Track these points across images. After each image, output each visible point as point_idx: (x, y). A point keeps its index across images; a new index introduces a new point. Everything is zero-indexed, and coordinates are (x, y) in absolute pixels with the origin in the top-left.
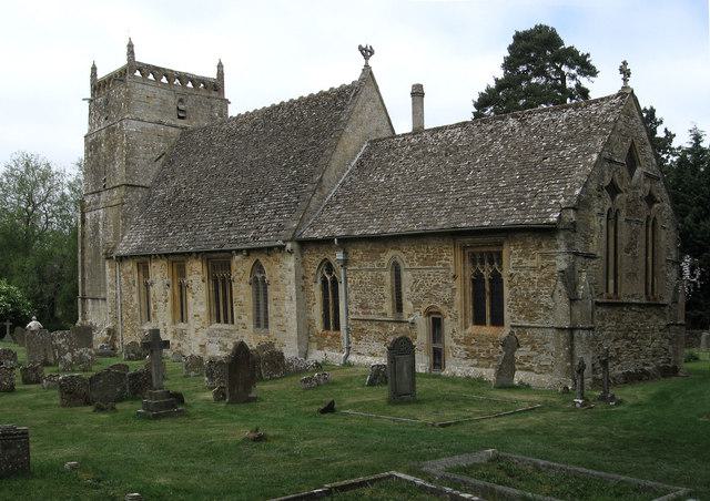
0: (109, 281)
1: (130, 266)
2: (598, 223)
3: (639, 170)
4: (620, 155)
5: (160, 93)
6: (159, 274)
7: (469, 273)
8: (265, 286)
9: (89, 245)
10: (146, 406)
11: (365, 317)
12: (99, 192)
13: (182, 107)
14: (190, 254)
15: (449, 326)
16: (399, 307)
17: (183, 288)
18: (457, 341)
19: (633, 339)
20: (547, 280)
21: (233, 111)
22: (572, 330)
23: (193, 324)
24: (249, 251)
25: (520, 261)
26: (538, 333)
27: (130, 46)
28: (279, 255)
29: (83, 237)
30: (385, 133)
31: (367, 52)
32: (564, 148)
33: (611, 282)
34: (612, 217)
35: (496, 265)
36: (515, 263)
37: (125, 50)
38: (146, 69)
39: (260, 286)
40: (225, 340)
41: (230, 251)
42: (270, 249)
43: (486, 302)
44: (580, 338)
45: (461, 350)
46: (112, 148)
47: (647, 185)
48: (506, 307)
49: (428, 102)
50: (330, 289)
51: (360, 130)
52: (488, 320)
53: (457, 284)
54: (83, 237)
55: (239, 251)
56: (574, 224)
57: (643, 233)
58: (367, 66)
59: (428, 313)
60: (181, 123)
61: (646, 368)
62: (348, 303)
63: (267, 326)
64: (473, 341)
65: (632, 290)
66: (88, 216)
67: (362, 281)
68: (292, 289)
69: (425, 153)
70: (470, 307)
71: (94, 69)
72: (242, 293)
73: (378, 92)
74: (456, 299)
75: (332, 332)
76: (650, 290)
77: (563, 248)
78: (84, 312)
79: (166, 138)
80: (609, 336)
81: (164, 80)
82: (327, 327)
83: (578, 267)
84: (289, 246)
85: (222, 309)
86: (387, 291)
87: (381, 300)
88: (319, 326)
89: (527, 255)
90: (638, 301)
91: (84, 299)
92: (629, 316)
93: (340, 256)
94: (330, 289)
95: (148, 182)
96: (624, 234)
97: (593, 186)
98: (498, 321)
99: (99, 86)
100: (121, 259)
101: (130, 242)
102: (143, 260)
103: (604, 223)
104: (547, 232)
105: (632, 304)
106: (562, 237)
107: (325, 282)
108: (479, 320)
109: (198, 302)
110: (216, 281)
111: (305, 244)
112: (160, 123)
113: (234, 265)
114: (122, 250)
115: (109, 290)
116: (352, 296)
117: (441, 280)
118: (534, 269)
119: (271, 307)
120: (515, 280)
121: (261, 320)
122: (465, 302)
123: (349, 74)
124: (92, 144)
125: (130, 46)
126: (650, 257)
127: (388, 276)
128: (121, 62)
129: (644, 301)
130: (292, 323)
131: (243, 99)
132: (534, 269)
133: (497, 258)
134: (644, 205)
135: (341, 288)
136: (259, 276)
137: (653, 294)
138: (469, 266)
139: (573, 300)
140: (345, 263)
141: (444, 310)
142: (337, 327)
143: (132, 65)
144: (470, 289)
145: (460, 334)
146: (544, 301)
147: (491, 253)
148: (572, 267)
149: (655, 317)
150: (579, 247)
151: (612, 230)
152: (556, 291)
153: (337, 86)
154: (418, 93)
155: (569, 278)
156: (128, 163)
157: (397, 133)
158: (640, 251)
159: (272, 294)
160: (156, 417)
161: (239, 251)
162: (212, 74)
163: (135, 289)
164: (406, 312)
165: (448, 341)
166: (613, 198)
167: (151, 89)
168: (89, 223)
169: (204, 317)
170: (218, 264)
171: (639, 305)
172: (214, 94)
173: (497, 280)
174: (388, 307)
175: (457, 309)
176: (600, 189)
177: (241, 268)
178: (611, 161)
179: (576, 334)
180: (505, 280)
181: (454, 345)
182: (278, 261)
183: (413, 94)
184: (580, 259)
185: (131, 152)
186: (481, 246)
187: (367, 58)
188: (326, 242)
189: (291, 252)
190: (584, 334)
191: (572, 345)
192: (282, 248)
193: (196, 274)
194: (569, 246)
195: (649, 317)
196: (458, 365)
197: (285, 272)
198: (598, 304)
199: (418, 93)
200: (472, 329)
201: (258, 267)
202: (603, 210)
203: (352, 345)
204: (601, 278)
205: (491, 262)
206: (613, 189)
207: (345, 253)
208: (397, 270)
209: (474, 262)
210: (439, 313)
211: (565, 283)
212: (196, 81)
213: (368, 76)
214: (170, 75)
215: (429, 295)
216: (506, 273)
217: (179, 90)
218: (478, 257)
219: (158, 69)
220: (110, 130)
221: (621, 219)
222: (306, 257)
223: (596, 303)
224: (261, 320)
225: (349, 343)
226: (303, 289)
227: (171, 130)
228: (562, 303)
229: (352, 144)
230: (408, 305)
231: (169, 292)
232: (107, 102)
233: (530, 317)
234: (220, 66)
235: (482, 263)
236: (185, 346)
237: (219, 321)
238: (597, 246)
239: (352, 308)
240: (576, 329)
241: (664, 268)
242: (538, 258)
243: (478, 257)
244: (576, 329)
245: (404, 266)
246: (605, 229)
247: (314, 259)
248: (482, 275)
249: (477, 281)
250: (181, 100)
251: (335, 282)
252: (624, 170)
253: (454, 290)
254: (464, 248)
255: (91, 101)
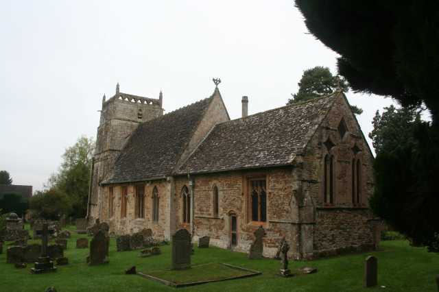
0: (99, 196)
1: (106, 189)
2: (318, 163)
3: (347, 133)
4: (334, 124)
5: (131, 107)
6: (117, 192)
7: (251, 191)
8: (158, 198)
9: (94, 179)
10: (36, 266)
11: (201, 216)
12: (100, 154)
13: (140, 113)
14: (129, 183)
15: (240, 221)
16: (216, 211)
17: (126, 199)
18: (243, 230)
19: (343, 229)
20: (287, 195)
21: (164, 113)
22: (300, 225)
23: (129, 218)
24: (153, 182)
25: (274, 186)
26: (283, 226)
27: (118, 86)
28: (164, 184)
29: (92, 175)
30: (225, 120)
31: (217, 82)
32: (303, 123)
33: (328, 196)
34: (328, 160)
35: (263, 188)
36: (275, 187)
37: (159, 95)
38: (124, 96)
39: (156, 199)
40: (140, 226)
41: (144, 181)
42: (161, 180)
43: (258, 209)
44: (305, 229)
45: (244, 235)
46: (106, 132)
47: (353, 142)
48: (267, 212)
49: (250, 104)
50: (187, 200)
51: (212, 120)
52: (259, 218)
53: (244, 198)
54: (92, 175)
55: (148, 182)
56: (302, 164)
57: (350, 167)
58: (217, 88)
59: (230, 214)
60: (140, 120)
61: (354, 246)
62: (194, 208)
63: (158, 220)
64: (251, 230)
65: (343, 200)
66: (95, 165)
67: (201, 194)
68: (168, 201)
69: (239, 129)
70: (250, 210)
71: (104, 97)
72: (149, 203)
73: (222, 101)
74: (242, 205)
75: (187, 224)
76: (356, 200)
77: (296, 177)
78: (90, 211)
79: (132, 127)
80: (327, 228)
81: (133, 101)
82: (184, 221)
83: (305, 188)
84: (168, 179)
85: (140, 212)
86: (211, 202)
87: (208, 207)
88: (181, 220)
89: (278, 182)
90: (347, 207)
91: (90, 204)
92: (341, 216)
93: (191, 183)
94: (187, 200)
95: (121, 148)
96: (337, 169)
97: (315, 142)
98: (264, 219)
99: (106, 105)
100: (104, 185)
101: (110, 177)
102: (111, 186)
103: (323, 163)
104: (288, 168)
105: (344, 209)
106: (295, 171)
107: (185, 197)
108: (255, 218)
109: (131, 208)
110: (139, 196)
111: (177, 178)
112: (129, 120)
113: (146, 188)
114: (105, 181)
115: (99, 201)
116: (196, 204)
117: (234, 195)
118: (281, 189)
119: (160, 210)
120: (272, 195)
121: (156, 217)
122: (248, 208)
123: (208, 94)
124: (100, 132)
125: (118, 86)
126: (356, 182)
127: (212, 193)
128: (113, 94)
129: (351, 206)
130: (168, 219)
131: (169, 107)
132: (281, 189)
133: (263, 184)
134: (352, 153)
135: (191, 199)
136: (156, 194)
137: (358, 201)
138: (250, 188)
139: (300, 208)
140: (194, 187)
141: (237, 212)
142: (189, 222)
143: (118, 94)
144: (251, 201)
145: (245, 226)
146: (286, 207)
147: (261, 181)
148: (301, 188)
149: (360, 216)
150: (305, 176)
151: (328, 167)
152: (292, 202)
153: (203, 99)
154: (245, 101)
155: (299, 195)
156: (112, 139)
157: (232, 119)
158: (349, 179)
159: (161, 203)
160: (41, 272)
161: (148, 182)
162: (157, 98)
163: (108, 200)
164: (220, 213)
165: (239, 230)
166: (329, 149)
167: (125, 105)
168: (95, 169)
169: (133, 214)
170: (140, 188)
171: (348, 209)
172: (157, 106)
173: (264, 195)
174: (211, 210)
175: (244, 211)
176: (320, 144)
177: (149, 189)
178: (327, 128)
179: (302, 227)
180: (267, 195)
181: (242, 232)
182: (164, 186)
183: (243, 101)
184: (305, 184)
185: (114, 134)
186: (256, 177)
187: (217, 84)
188: (184, 176)
189: (169, 182)
190: (307, 227)
191: (300, 233)
192: (165, 180)
193: (131, 191)
194: (299, 176)
195: (355, 216)
196: (243, 243)
197: (167, 191)
198: (318, 209)
199: (245, 101)
200: (251, 223)
201: (155, 190)
202: (322, 155)
203: (195, 231)
204: (321, 194)
205: (261, 186)
206: (329, 144)
207: (194, 182)
208: (216, 190)
209: (253, 185)
210: (235, 214)
211: (296, 198)
212: (149, 101)
213: (217, 92)
214: (136, 98)
215: (230, 204)
216: (268, 191)
217: (139, 105)
218: (255, 183)
219: (130, 96)
220: (107, 124)
221: (335, 160)
222: (177, 184)
223: (317, 208)
224: (156, 217)
225: (194, 229)
226: (174, 201)
227: (134, 123)
228: (294, 209)
229: (206, 126)
230: (221, 209)
231: (120, 202)
232: (107, 112)
233: (279, 217)
234: (161, 94)
235: (257, 187)
236: (125, 229)
237: (139, 217)
238: (318, 174)
239: (196, 211)
240: (303, 224)
241: (366, 188)
242: (283, 182)
243: (255, 183)
244: (303, 224)
245: (220, 188)
246: (323, 167)
247: (180, 185)
248: (256, 193)
249: (254, 196)
250: (140, 110)
251: (189, 198)
252: (338, 135)
253: (242, 202)
254: (248, 179)
255: (102, 112)
